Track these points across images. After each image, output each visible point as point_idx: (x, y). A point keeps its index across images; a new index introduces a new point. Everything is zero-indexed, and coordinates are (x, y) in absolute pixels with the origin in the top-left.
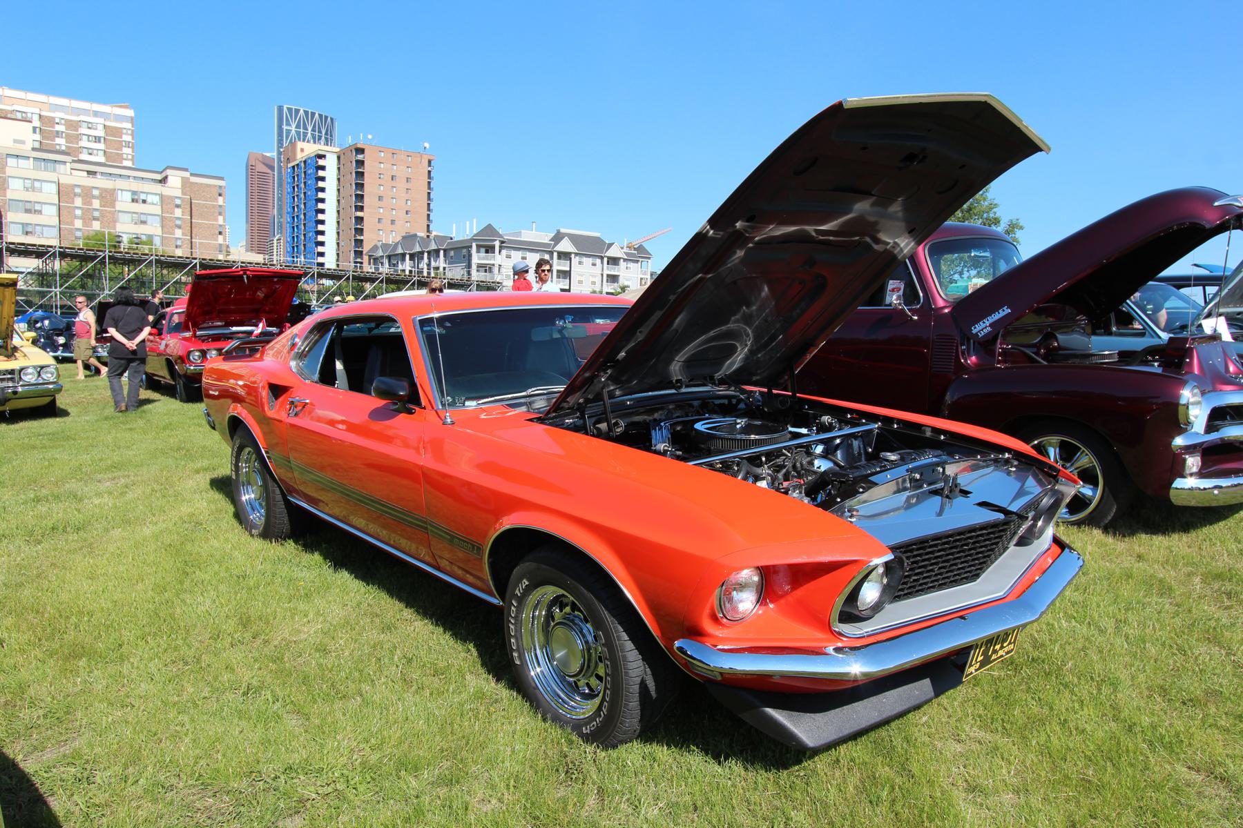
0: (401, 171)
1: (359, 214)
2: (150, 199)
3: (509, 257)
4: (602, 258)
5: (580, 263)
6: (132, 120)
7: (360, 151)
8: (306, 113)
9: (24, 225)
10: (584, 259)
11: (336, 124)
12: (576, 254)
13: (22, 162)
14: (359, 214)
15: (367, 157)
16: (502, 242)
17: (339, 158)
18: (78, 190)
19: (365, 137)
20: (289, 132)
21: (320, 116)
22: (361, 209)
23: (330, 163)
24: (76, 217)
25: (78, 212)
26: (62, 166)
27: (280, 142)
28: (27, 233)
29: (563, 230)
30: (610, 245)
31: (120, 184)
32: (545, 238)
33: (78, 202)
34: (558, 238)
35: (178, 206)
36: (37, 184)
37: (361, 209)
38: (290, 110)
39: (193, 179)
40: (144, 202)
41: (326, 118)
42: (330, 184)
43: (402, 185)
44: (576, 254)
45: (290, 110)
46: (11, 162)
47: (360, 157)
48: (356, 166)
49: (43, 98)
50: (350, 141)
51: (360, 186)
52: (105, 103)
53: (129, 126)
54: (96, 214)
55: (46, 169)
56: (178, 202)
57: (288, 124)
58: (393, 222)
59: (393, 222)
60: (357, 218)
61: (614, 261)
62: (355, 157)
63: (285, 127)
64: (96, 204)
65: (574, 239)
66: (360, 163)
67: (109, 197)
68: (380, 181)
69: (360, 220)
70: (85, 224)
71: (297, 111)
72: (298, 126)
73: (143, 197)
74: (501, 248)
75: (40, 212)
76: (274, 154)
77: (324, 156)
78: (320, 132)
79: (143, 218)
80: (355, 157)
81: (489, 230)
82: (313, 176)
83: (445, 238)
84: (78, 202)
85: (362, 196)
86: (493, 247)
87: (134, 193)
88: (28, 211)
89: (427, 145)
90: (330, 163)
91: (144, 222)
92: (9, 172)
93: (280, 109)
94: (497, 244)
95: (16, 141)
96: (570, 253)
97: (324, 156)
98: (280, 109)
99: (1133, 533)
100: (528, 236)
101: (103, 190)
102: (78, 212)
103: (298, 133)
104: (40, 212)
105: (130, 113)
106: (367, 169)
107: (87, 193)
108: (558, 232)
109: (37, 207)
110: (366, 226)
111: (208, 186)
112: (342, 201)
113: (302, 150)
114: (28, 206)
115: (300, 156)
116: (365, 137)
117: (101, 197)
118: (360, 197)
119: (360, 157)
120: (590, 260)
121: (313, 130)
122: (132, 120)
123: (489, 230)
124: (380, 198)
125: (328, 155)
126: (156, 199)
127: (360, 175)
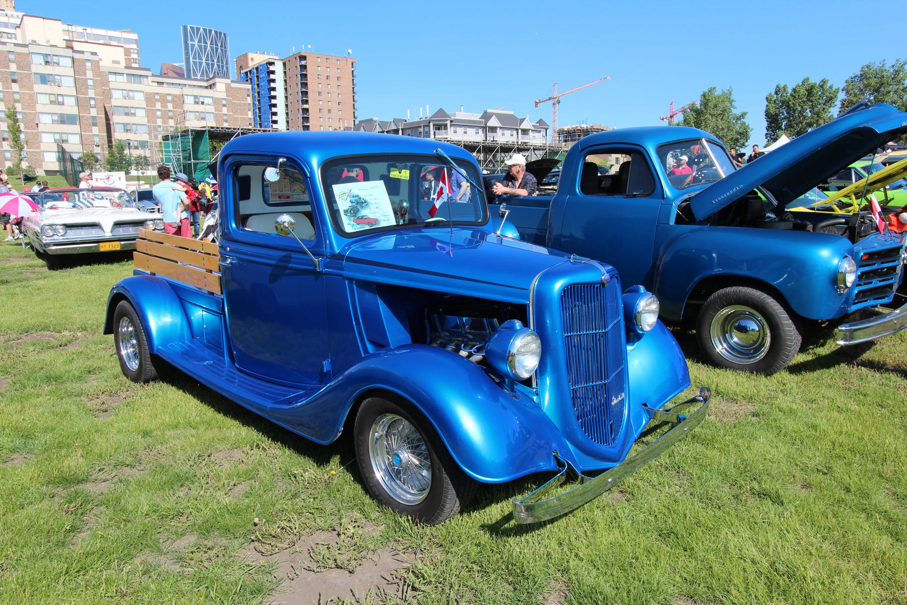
0: (333, 72)
1: (305, 106)
2: (206, 101)
3: (455, 132)
4: (517, 130)
5: (503, 134)
6: (136, 42)
7: (303, 58)
8: (205, 30)
9: (125, 125)
10: (506, 132)
11: (228, 38)
12: (501, 128)
13: (119, 78)
14: (305, 106)
15: (309, 63)
16: (451, 121)
17: (284, 64)
18: (157, 97)
19: (306, 47)
20: (193, 46)
21: (216, 32)
22: (306, 102)
23: (278, 68)
24: (158, 117)
25: (159, 113)
26: (145, 79)
27: (187, 54)
28: (127, 131)
29: (489, 111)
30: (522, 120)
31: (187, 91)
32: (476, 117)
33: (158, 106)
34: (487, 116)
35: (224, 105)
36: (131, 94)
37: (306, 102)
38: (192, 28)
39: (233, 85)
40: (203, 103)
41: (220, 33)
42: (279, 85)
43: (334, 83)
44: (501, 128)
45: (192, 28)
46: (111, 78)
47: (303, 63)
48: (300, 68)
49: (102, 32)
50: (294, 51)
51: (304, 85)
52: (115, 29)
53: (135, 46)
54: (171, 114)
55: (135, 82)
56: (224, 102)
57: (192, 40)
58: (329, 111)
59: (329, 111)
60: (303, 109)
61: (525, 132)
62: (298, 63)
63: (190, 42)
64: (170, 106)
65: (500, 117)
66: (304, 67)
67: (179, 101)
68: (319, 81)
69: (306, 111)
70: (164, 122)
71: (198, 29)
72: (200, 41)
73: (201, 100)
74: (451, 125)
75: (134, 114)
76: (183, 64)
77: (273, 63)
78: (217, 45)
79: (203, 115)
80: (298, 63)
81: (441, 112)
82: (266, 79)
83: (401, 120)
84: (158, 106)
85: (306, 93)
86: (446, 126)
87: (196, 97)
88: (127, 114)
89: (350, 51)
90: (278, 68)
91: (203, 119)
92: (112, 85)
93: (185, 28)
94: (448, 123)
95: (114, 62)
96: (496, 128)
97: (273, 63)
98: (185, 28)
99: (698, 362)
100: (461, 115)
101: (174, 96)
102: (159, 113)
103: (200, 47)
104: (134, 114)
105: (134, 36)
106: (309, 71)
107: (163, 99)
108: (486, 112)
109: (133, 111)
110: (312, 115)
111: (240, 89)
112: (290, 97)
113: (252, 59)
114: (127, 110)
115: (251, 65)
116: (306, 47)
117: (173, 101)
118: (305, 94)
119: (303, 63)
120: (474, 130)
121: (211, 44)
122: (136, 42)
123: (441, 112)
124: (320, 93)
125: (276, 62)
126: (210, 101)
127: (304, 76)
